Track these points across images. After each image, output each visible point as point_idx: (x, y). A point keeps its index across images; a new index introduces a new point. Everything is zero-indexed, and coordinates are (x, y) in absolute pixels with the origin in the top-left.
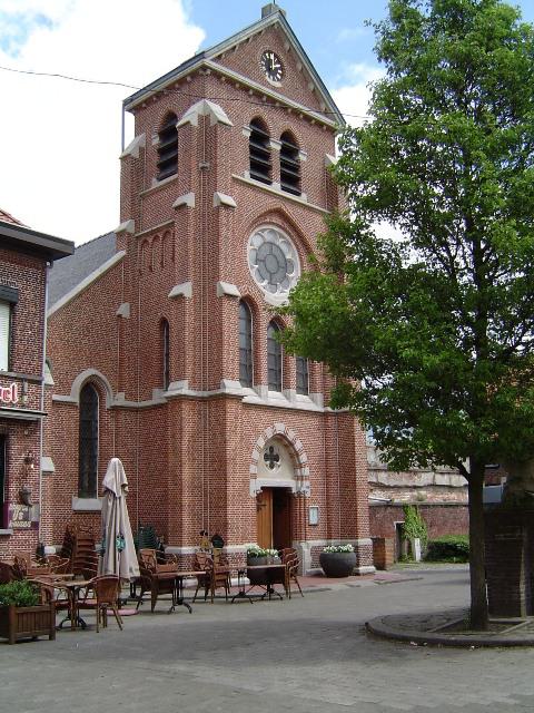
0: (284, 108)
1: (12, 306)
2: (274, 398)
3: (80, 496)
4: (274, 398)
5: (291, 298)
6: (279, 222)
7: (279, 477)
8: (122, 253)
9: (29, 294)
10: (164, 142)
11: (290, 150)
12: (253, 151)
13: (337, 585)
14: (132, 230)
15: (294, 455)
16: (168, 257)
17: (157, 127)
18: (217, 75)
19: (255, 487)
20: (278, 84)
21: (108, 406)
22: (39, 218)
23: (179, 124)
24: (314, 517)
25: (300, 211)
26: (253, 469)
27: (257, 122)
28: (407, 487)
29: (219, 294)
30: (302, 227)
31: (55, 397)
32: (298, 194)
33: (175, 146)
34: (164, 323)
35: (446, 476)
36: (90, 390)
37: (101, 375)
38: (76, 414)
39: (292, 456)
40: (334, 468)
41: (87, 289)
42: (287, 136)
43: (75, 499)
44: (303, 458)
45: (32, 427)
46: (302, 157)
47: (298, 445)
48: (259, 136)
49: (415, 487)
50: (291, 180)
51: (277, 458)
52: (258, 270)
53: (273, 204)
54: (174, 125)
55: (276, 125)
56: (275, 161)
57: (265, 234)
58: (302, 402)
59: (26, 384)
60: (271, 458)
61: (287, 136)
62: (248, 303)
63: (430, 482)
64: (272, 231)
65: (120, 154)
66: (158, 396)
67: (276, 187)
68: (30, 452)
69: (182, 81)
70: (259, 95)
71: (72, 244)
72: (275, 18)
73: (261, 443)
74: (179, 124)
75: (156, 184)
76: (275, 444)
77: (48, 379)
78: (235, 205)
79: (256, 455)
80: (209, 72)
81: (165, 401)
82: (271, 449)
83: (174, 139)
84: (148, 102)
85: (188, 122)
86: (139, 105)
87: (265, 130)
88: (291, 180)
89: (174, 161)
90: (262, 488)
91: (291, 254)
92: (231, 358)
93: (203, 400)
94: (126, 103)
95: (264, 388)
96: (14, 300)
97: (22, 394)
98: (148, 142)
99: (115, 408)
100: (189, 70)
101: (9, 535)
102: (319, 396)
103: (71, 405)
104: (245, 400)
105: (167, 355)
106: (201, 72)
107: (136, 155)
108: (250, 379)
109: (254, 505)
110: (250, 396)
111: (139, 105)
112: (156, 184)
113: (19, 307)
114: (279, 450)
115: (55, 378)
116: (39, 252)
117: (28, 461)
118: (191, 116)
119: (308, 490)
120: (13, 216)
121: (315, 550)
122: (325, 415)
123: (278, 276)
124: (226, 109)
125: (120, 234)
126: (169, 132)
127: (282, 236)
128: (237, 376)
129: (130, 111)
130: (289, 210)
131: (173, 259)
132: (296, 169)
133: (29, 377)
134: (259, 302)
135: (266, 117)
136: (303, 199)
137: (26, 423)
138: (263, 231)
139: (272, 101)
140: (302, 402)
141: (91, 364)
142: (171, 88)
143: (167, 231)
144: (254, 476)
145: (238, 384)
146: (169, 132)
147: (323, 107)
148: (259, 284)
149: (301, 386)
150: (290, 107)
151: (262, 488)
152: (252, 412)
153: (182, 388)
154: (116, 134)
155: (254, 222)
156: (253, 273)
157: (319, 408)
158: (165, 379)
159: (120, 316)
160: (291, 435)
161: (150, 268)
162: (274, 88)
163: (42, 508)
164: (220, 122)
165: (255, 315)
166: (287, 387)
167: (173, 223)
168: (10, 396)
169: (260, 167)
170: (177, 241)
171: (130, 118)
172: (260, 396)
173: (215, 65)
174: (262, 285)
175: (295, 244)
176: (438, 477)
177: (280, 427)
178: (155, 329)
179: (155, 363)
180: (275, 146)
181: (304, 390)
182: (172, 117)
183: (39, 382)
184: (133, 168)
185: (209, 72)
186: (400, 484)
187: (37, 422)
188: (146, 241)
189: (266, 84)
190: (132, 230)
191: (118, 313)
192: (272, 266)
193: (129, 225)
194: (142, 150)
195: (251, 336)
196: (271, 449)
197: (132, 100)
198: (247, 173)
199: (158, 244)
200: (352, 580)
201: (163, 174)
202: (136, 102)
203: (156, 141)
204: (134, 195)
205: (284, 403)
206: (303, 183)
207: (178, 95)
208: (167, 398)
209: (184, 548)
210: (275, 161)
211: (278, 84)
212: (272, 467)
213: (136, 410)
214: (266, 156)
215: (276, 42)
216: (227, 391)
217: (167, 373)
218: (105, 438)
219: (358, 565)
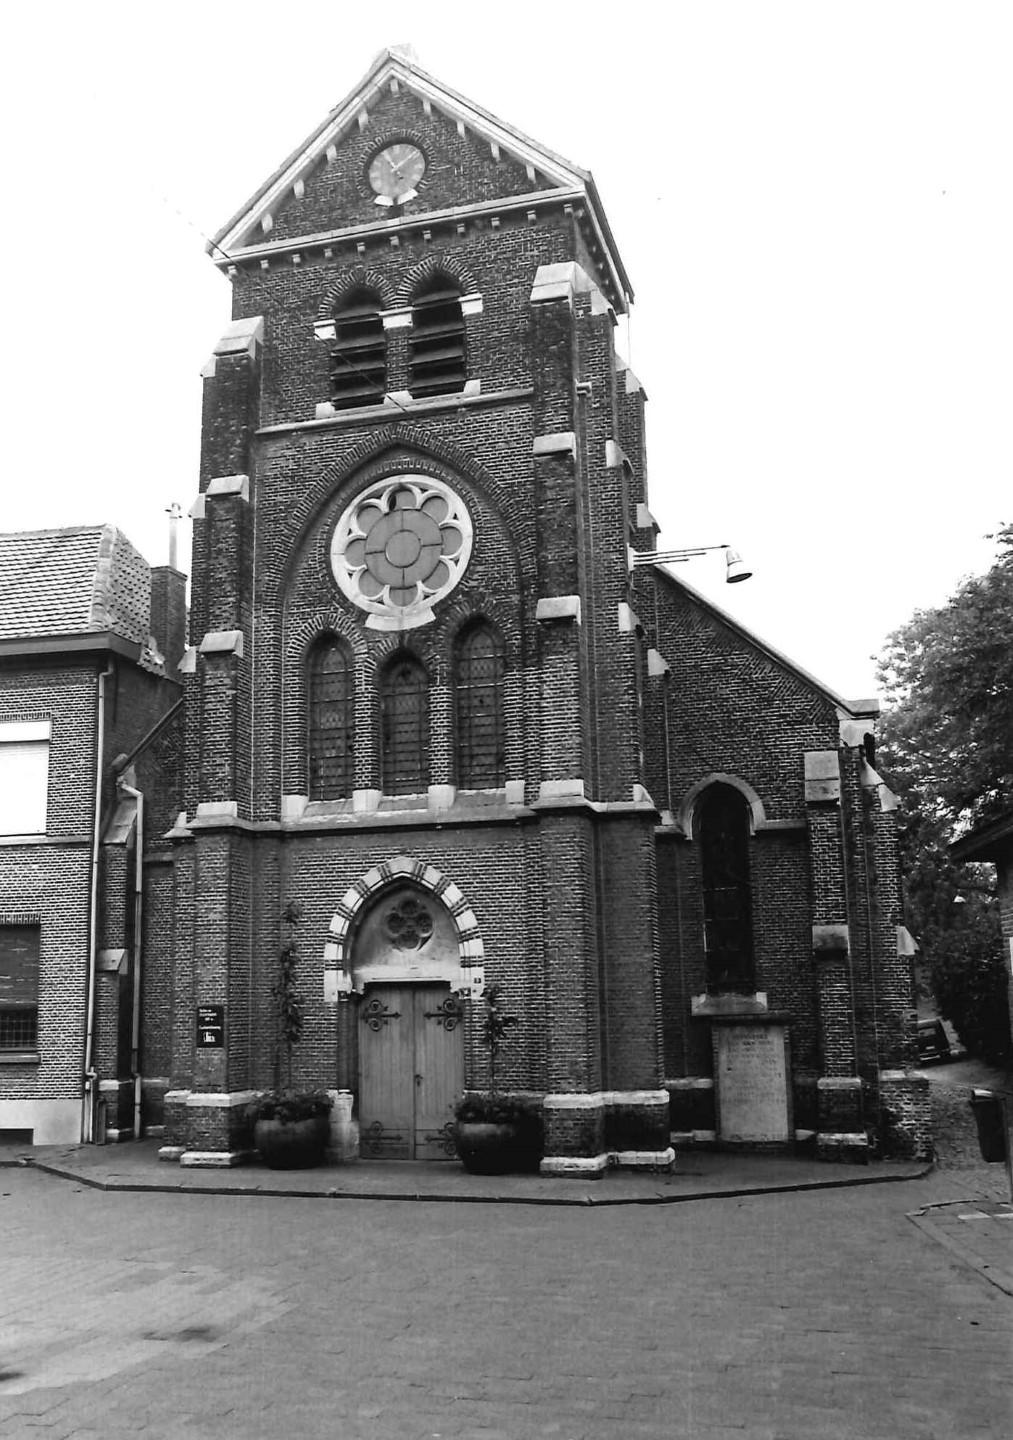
177: (402, 866)
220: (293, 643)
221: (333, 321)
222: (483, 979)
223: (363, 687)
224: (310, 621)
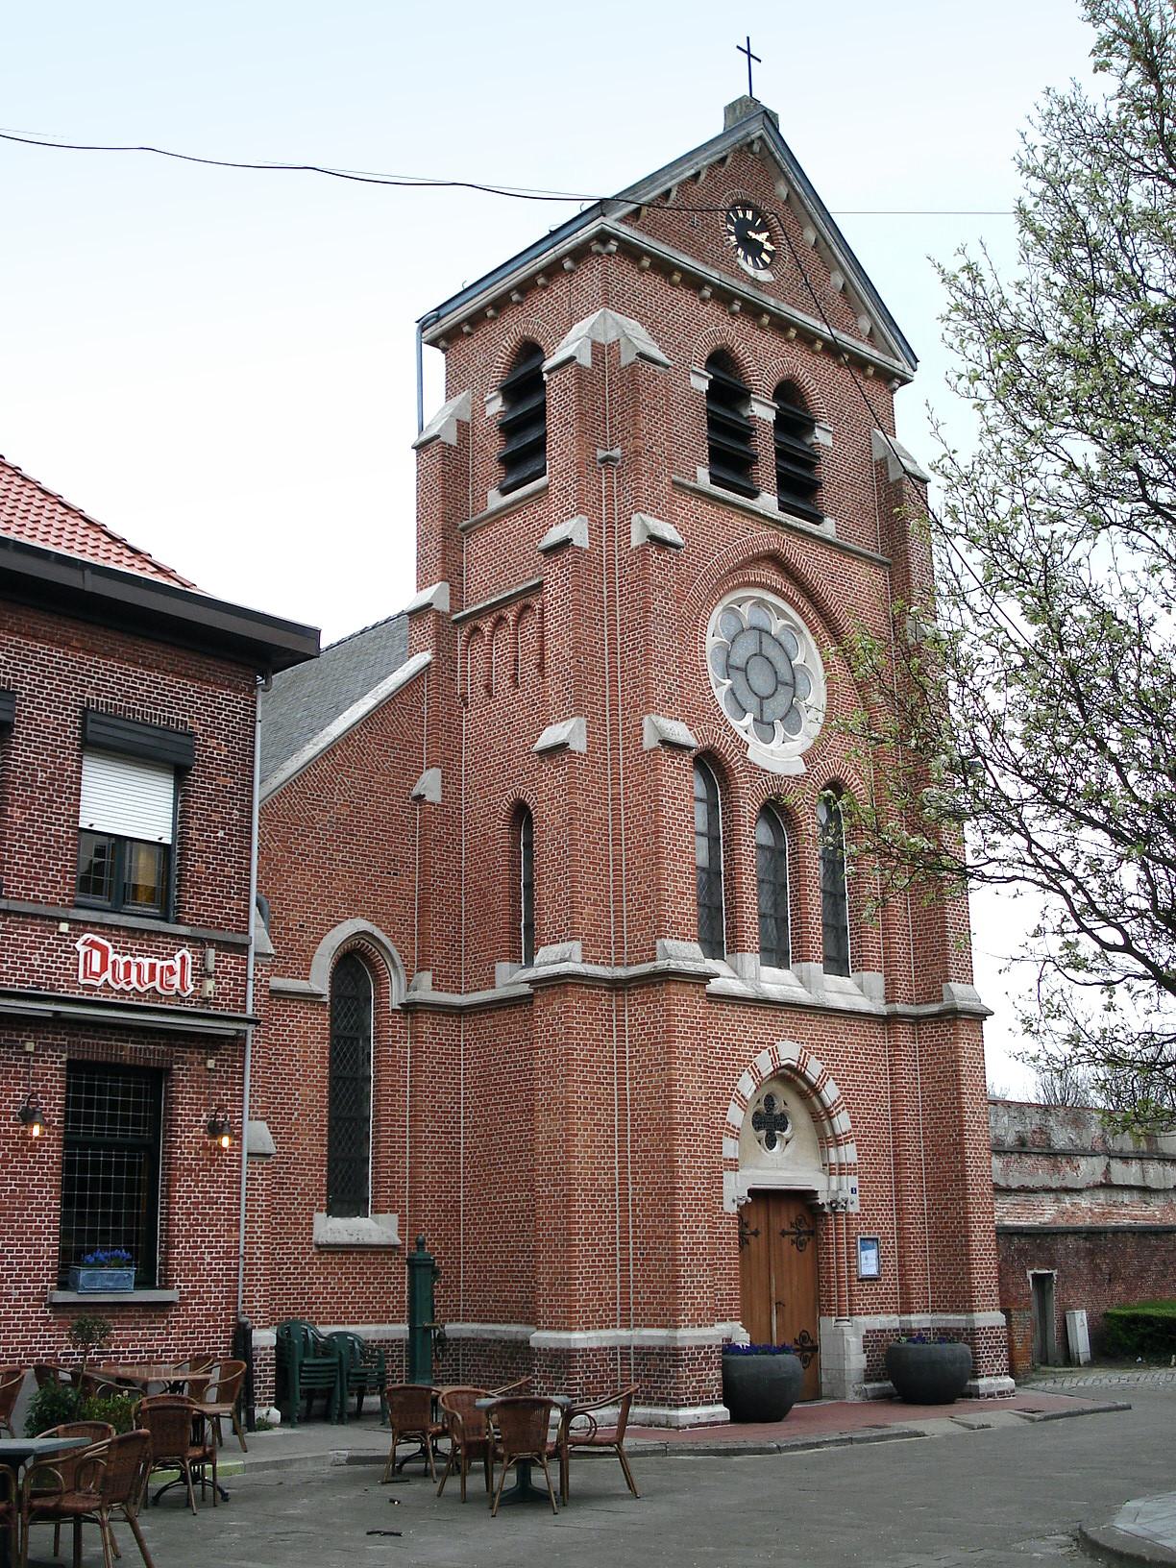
0: (781, 325)
1: (180, 773)
2: (778, 983)
3: (331, 1211)
4: (778, 983)
5: (808, 758)
6: (776, 579)
7: (788, 1166)
8: (423, 658)
9: (216, 748)
10: (512, 408)
11: (794, 419)
12: (715, 424)
13: (934, 1423)
14: (443, 605)
15: (821, 1116)
16: (528, 668)
17: (496, 375)
18: (631, 252)
19: (735, 1188)
20: (764, 276)
21: (394, 1004)
22: (226, 565)
23: (548, 364)
24: (868, 1263)
25: (823, 555)
26: (730, 1148)
27: (721, 361)
28: (1048, 1190)
29: (650, 741)
30: (828, 592)
31: (277, 983)
32: (817, 519)
33: (539, 415)
34: (521, 814)
35: (1135, 1167)
36: (356, 965)
37: (377, 932)
38: (322, 1020)
39: (815, 1117)
40: (915, 1148)
41: (347, 737)
42: (787, 392)
43: (320, 1218)
44: (843, 1122)
45: (226, 1050)
46: (822, 437)
47: (831, 1092)
48: (728, 388)
49: (1068, 1190)
50: (800, 488)
51: (782, 1122)
52: (732, 690)
53: (765, 539)
54: (539, 367)
55: (765, 361)
56: (765, 447)
57: (745, 610)
58: (843, 992)
59: (212, 952)
60: (769, 1124)
61: (787, 392)
62: (711, 764)
63: (1100, 1179)
64: (760, 603)
65: (414, 438)
66: (510, 978)
67: (767, 502)
68: (220, 1108)
69: (553, 271)
70: (724, 297)
71: (315, 634)
72: (756, 130)
73: (747, 1086)
74: (548, 364)
75: (495, 500)
76: (777, 1087)
77: (258, 935)
78: (679, 540)
79: (736, 1116)
80: (613, 246)
81: (526, 989)
82: (770, 1100)
83: (534, 402)
84: (476, 319)
85: (572, 359)
86: (450, 331)
87: (806, 410)
88: (800, 488)
89: (539, 447)
90: (751, 1192)
91: (808, 654)
92: (683, 901)
93: (616, 986)
94: (424, 325)
95: (750, 960)
96: (187, 761)
97: (202, 974)
98: (478, 409)
99: (410, 1009)
100: (567, 245)
101: (168, 1305)
102: (875, 980)
103: (311, 998)
104: (714, 986)
105: (529, 886)
106: (596, 247)
107: (451, 438)
108: (717, 941)
109: (734, 1233)
110: (727, 979)
111: (450, 331)
112: (495, 500)
113: (195, 776)
114: (788, 1103)
115: (273, 939)
116: (252, 650)
117: (215, 1130)
118: (572, 344)
119: (856, 1198)
120: (156, 558)
121: (873, 1340)
122: (889, 1020)
123: (777, 706)
124: (652, 327)
125: (417, 614)
126: (525, 384)
127: (782, 614)
128: (694, 931)
129: (433, 343)
130: (798, 554)
131: (541, 667)
132: (810, 460)
133: (217, 935)
134: (734, 761)
135: (741, 350)
136: (828, 528)
137: (211, 1043)
138: (741, 602)
139: (753, 311)
140: (843, 992)
141: (373, 916)
142: (526, 287)
143: (526, 601)
144: (734, 1165)
145: (695, 949)
146: (525, 384)
147: (865, 324)
148: (732, 721)
149: (833, 954)
150: (847, 351)
151: (751, 1192)
152: (727, 1011)
153: (558, 957)
154: (412, 396)
155: (721, 582)
156: (720, 694)
157: (872, 1003)
158: (524, 942)
159: (420, 798)
160: (814, 1069)
161: (488, 687)
162: (755, 283)
163: (250, 1234)
164: (641, 355)
165: (727, 789)
166: (736, 947)
167: (541, 584)
168: (176, 980)
169: (731, 460)
170: (551, 626)
171: (435, 357)
172: (742, 978)
173: (626, 231)
174: (743, 726)
175: (814, 632)
176: (1117, 1166)
177: (789, 1051)
178: (499, 827)
179: (500, 903)
180: (763, 411)
181: (837, 964)
182: (530, 351)
183: (244, 948)
184: (444, 463)
185: (613, 246)
186: (1030, 1182)
187: (238, 1040)
188: (476, 630)
189: (740, 274)
190: (443, 605)
191: (415, 792)
192: (762, 681)
193: (435, 593)
194: (463, 427)
195: (720, 838)
196: (770, 1100)
197: (438, 318)
198: (703, 476)
199: (505, 634)
200: (970, 1414)
201: (510, 481)
202: (447, 322)
203: (496, 406)
204: (449, 532)
205: (801, 995)
206: (826, 497)
207: (541, 300)
208: (531, 982)
209: (681, 1333)
210: (765, 447)
211: (764, 276)
212: (771, 1143)
213: (460, 1011)
214: (744, 432)
215: (750, 174)
216: (673, 965)
217: (529, 926)
218: (388, 1078)
219: (976, 1376)
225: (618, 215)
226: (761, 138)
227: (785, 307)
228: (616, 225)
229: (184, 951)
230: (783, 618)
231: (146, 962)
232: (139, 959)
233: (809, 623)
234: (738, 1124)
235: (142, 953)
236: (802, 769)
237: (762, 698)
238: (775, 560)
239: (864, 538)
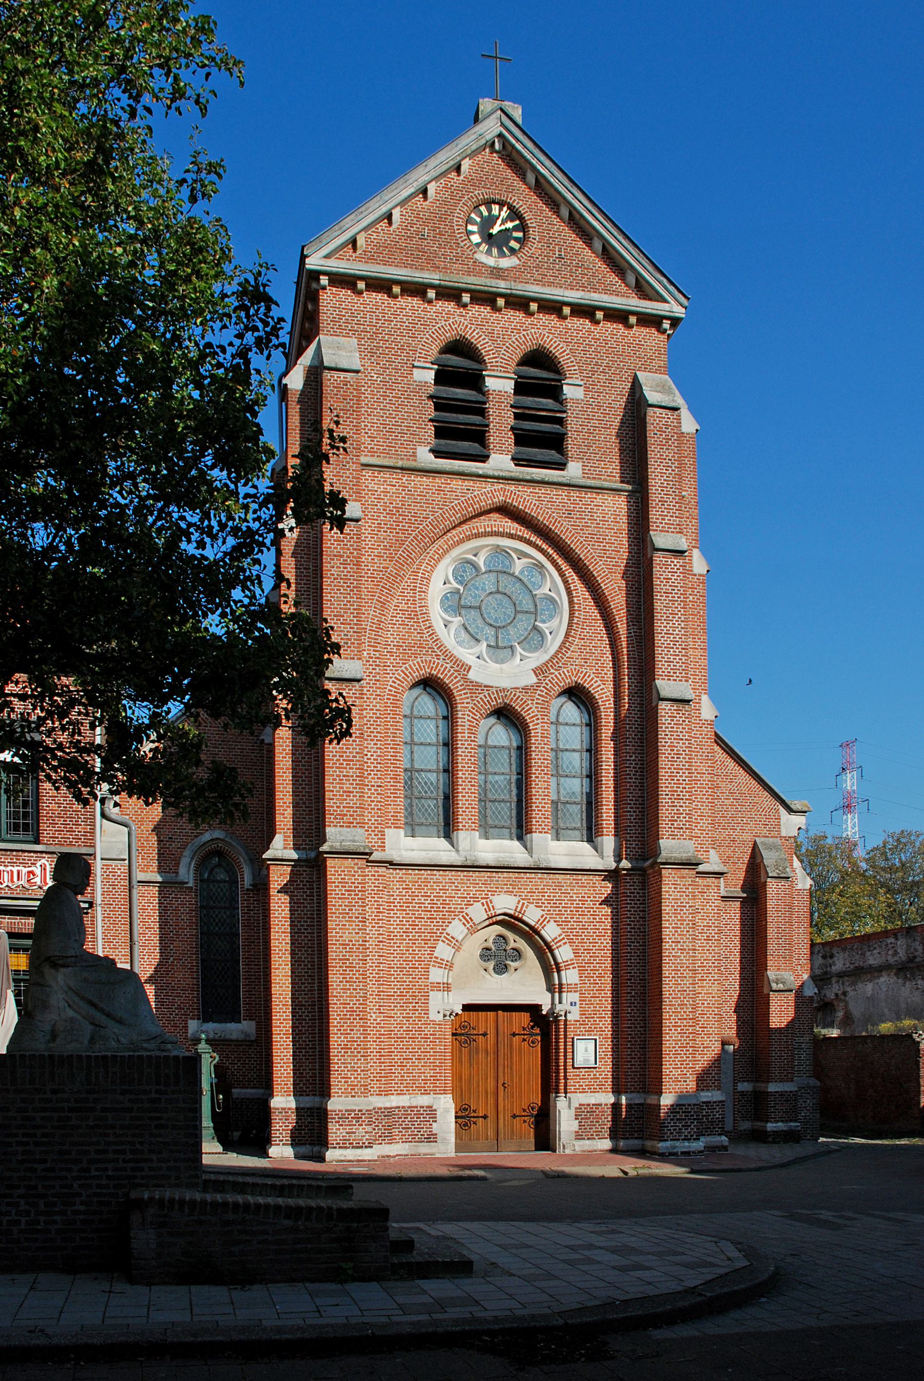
55: (502, 341)
67: (501, 461)
91: (552, 583)
136: (574, 470)
160: (532, 916)
168: (38, 880)
177: (505, 903)
220: (393, 682)
221: (513, 376)
222: (578, 1003)
223: (466, 735)
224: (411, 663)
225: (325, 251)
226: (500, 136)
227: (513, 285)
228: (323, 262)
229: (43, 861)
230: (525, 556)
231: (15, 869)
232: (9, 868)
233: (548, 557)
234: (48, 863)
235: (12, 864)
236: (533, 680)
237: (497, 628)
238: (505, 510)
239: (611, 471)
